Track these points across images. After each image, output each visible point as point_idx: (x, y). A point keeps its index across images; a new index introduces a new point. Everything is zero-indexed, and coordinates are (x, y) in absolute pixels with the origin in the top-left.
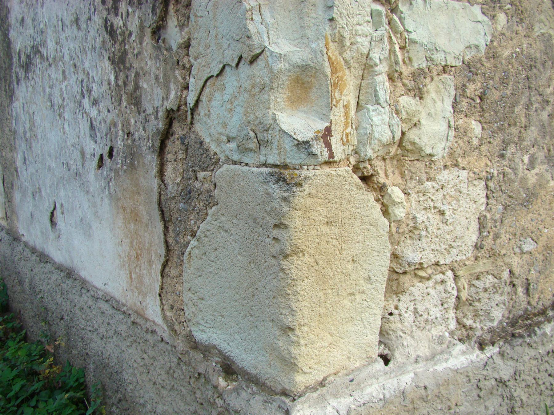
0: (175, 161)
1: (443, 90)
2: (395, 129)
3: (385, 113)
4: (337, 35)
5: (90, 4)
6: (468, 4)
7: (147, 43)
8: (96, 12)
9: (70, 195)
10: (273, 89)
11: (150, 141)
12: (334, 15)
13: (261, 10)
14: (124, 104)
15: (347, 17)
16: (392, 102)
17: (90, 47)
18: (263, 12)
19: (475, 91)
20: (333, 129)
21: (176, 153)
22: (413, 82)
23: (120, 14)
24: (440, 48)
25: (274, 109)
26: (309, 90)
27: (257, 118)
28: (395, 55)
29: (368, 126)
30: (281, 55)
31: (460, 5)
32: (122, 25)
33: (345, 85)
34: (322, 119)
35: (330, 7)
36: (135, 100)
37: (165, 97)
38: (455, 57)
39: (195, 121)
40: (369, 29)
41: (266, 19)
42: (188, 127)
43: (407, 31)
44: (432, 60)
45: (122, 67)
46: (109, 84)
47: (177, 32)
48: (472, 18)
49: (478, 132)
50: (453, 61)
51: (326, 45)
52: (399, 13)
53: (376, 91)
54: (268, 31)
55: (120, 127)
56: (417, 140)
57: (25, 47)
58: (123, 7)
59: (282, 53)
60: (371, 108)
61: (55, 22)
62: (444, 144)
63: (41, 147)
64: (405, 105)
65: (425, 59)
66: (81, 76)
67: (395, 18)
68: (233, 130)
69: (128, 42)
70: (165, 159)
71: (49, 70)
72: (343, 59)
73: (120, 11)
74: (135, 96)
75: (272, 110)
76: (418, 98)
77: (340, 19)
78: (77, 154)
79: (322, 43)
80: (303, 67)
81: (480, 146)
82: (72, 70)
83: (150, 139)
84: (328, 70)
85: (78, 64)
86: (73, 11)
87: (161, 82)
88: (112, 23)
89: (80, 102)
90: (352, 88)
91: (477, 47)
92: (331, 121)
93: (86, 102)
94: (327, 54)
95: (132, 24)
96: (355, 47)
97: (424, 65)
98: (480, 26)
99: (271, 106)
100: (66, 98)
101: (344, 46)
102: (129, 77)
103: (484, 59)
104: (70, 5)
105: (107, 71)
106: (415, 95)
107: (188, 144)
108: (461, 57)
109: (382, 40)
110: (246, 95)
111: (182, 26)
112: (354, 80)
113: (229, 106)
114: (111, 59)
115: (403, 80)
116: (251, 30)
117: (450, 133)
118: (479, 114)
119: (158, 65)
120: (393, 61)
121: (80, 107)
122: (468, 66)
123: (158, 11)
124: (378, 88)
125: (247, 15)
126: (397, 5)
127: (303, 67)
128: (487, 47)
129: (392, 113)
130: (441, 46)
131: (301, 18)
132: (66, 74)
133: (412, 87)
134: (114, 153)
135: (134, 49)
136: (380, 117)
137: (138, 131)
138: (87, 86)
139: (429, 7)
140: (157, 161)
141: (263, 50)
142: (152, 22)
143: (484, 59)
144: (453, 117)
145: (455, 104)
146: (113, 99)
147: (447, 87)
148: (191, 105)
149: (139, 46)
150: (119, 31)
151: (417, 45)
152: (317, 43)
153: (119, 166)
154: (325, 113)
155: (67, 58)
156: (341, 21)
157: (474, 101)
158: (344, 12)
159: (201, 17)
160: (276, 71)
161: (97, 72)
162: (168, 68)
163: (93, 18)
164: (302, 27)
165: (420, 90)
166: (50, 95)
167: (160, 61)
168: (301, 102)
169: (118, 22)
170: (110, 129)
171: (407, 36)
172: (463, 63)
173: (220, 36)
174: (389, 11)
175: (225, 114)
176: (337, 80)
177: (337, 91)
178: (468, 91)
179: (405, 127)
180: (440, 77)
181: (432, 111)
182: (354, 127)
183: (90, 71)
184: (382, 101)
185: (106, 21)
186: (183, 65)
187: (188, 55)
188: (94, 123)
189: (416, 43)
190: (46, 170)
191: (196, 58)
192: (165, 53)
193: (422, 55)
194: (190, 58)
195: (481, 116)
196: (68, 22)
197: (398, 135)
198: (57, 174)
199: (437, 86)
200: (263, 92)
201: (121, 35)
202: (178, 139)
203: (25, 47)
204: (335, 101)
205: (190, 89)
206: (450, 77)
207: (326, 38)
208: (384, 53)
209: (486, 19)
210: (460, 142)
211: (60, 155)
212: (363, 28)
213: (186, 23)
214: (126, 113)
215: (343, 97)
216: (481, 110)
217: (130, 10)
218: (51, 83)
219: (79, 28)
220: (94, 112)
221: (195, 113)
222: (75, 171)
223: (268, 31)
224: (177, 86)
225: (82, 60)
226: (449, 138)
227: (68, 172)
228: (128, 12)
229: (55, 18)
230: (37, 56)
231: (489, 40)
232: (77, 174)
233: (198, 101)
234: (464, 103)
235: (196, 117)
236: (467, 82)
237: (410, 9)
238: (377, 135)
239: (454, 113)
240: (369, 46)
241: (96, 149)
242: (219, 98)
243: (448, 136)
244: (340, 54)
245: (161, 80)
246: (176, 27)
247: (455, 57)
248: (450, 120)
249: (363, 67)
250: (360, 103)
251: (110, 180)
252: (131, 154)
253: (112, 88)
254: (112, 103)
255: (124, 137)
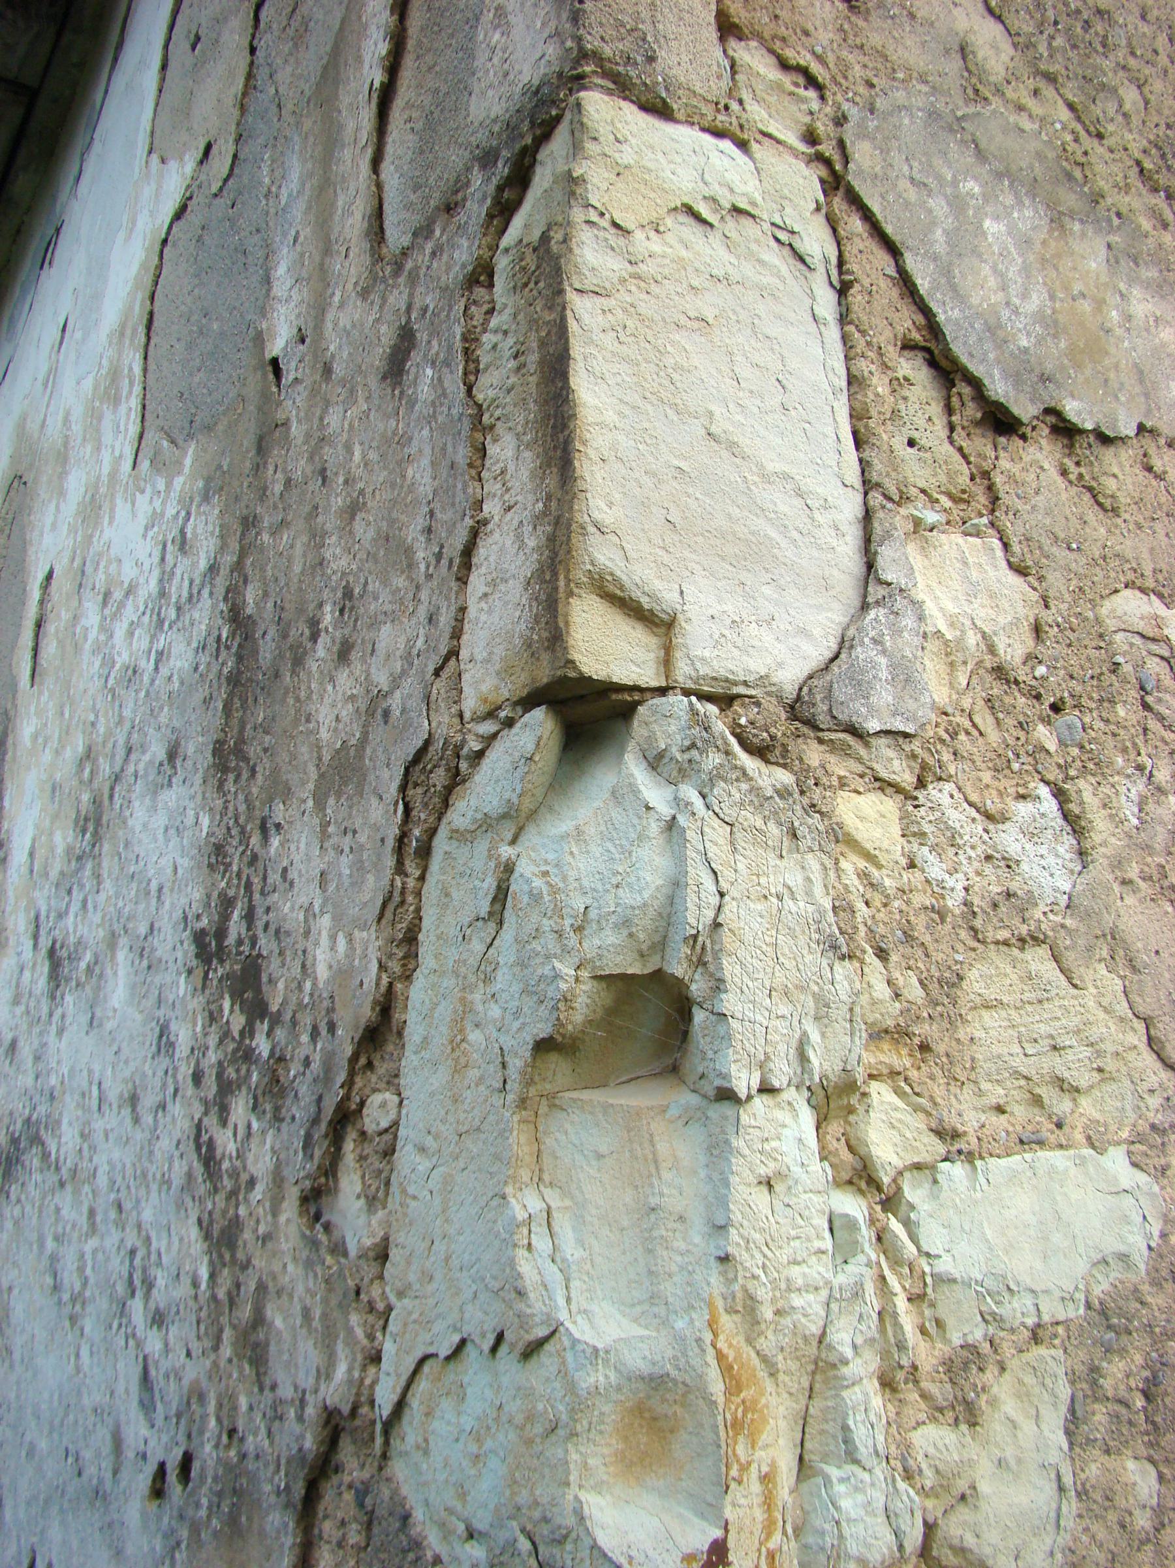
0: (340, 1545)
1: (1037, 1390)
2: (904, 1523)
3: (873, 1484)
4: (739, 1295)
5: (166, 1072)
6: (1092, 1152)
7: (288, 1220)
8: (178, 1099)
9: (75, 1544)
10: (577, 1435)
11: (282, 1473)
12: (730, 1249)
13: (553, 1224)
14: (227, 1351)
15: (765, 1249)
16: (893, 1449)
17: (158, 1176)
18: (556, 1228)
19: (1128, 1376)
20: (731, 1543)
21: (343, 1523)
22: (948, 1386)
23: (231, 1126)
24: (1018, 1284)
25: (580, 1487)
26: (668, 1435)
27: (538, 1504)
28: (897, 1325)
29: (827, 1526)
30: (596, 1350)
31: (1069, 1158)
32: (234, 1154)
33: (764, 1420)
34: (702, 1516)
35: (721, 1227)
36: (253, 1350)
37: (323, 1370)
38: (1063, 1299)
39: (392, 1453)
40: (822, 1270)
41: (564, 1246)
42: (376, 1464)
43: (928, 1255)
44: (998, 1319)
45: (227, 1257)
46: (195, 1284)
47: (360, 1209)
48: (1103, 1186)
49: (1146, 1491)
50: (1060, 1308)
51: (712, 1325)
52: (904, 1208)
53: (845, 1428)
54: (567, 1280)
55: (212, 1407)
56: (970, 1541)
57: (11, 1114)
58: (240, 1110)
59: (600, 1346)
60: (834, 1472)
61: (85, 1084)
62: (1049, 1541)
63: (18, 1383)
64: (931, 1451)
65: (979, 1318)
66: (132, 1239)
67: (895, 1225)
68: (480, 1513)
69: (245, 1198)
70: (316, 1531)
71: (57, 1195)
72: (758, 1353)
73: (233, 1119)
74: (253, 1338)
75: (574, 1489)
76: (964, 1427)
77: (745, 1256)
78: (103, 1436)
79: (700, 1318)
80: (651, 1380)
81: (1157, 1530)
82: (113, 1214)
83: (283, 1468)
84: (717, 1387)
85: (127, 1205)
86: (127, 1073)
87: (316, 1330)
88: (211, 1139)
89: (124, 1304)
90: (782, 1424)
91: (1123, 1257)
92: (727, 1523)
93: (137, 1306)
94: (714, 1346)
95: (256, 1161)
96: (787, 1321)
97: (977, 1334)
98: (1128, 1201)
99: (572, 1478)
100: (92, 1281)
101: (758, 1323)
102: (243, 1288)
103: (1145, 1288)
104: (123, 1057)
105: (192, 1251)
106: (956, 1419)
107: (373, 1511)
108: (1080, 1296)
109: (857, 1293)
110: (512, 1436)
111: (373, 1201)
112: (788, 1403)
113: (473, 1448)
114: (205, 1224)
115: (923, 1384)
116: (526, 1276)
117: (1064, 1509)
118: (1146, 1438)
119: (311, 1285)
120: (892, 1340)
121: (121, 1316)
122: (1104, 1313)
123: (318, 1153)
124: (851, 1423)
125: (516, 1237)
126: (899, 1189)
127: (651, 1380)
128: (1153, 1255)
129: (894, 1481)
130: (1020, 1278)
131: (650, 1251)
132: (99, 1218)
133: (946, 1400)
134: (193, 1474)
135: (258, 1221)
136: (860, 1498)
137: (256, 1434)
138: (144, 1270)
139: (983, 1181)
140: (295, 1536)
141: (553, 1333)
142: (302, 1174)
143: (1145, 1288)
144: (1068, 1462)
145: (1073, 1423)
146: (202, 1327)
147: (1048, 1381)
148: (386, 1413)
149: (269, 1218)
150: (226, 1165)
151: (955, 1287)
152: (687, 1318)
153: (203, 1513)
154: (709, 1498)
155: (102, 1180)
156: (749, 1261)
157: (1127, 1406)
158: (757, 1236)
159: (415, 1198)
160: (584, 1393)
161: (169, 1244)
162: (334, 1302)
163: (169, 1106)
164: (651, 1273)
165: (969, 1406)
166: (54, 1258)
167: (316, 1275)
168: (651, 1465)
169: (226, 1142)
170: (188, 1403)
171: (927, 1269)
172: (1088, 1306)
173: (455, 1262)
174: (878, 1208)
175: (464, 1463)
176: (740, 1410)
177: (741, 1438)
178: (1107, 1384)
179: (935, 1508)
180: (1028, 1357)
181: (1009, 1453)
182: (790, 1531)
183: (153, 1235)
184: (863, 1452)
185: (199, 1127)
186: (369, 1302)
187: (381, 1277)
188: (153, 1372)
189: (954, 1281)
190: (24, 1453)
191: (400, 1294)
192: (329, 1260)
193: (970, 1309)
194: (388, 1289)
195: (1150, 1444)
196: (112, 1095)
197: (914, 1536)
198: (49, 1474)
199: (1020, 1382)
200: (553, 1438)
201: (230, 1176)
202: (350, 1487)
203: (11, 1114)
204: (735, 1467)
205: (385, 1364)
206: (1053, 1352)
207: (711, 1305)
208: (863, 1328)
209: (1142, 1178)
210: (1095, 1528)
211: (62, 1424)
212: (807, 1270)
213: (381, 1194)
214: (230, 1376)
215: (760, 1454)
216: (1150, 1427)
217: (255, 1125)
218: (60, 1230)
219: (136, 1120)
220: (154, 1343)
221: (394, 1433)
222: (95, 1482)
223: (567, 1280)
224: (354, 1353)
225: (138, 1201)
226: (1062, 1523)
227: (76, 1479)
228: (249, 1126)
229: (85, 1073)
230: (34, 1150)
231: (1156, 1234)
232: (98, 1494)
233: (400, 1406)
234: (1097, 1417)
235: (395, 1443)
236: (1102, 1359)
237: (934, 1197)
238: (853, 1547)
239: (1071, 1449)
240: (823, 1314)
241: (152, 1443)
242: (450, 1416)
243: (1058, 1516)
244: (749, 1341)
245: (316, 1323)
246: (358, 1197)
247: (1063, 1299)
248: (1062, 1471)
249: (811, 1367)
250: (806, 1457)
251: (178, 1544)
252: (235, 1491)
253: (200, 1297)
254: (199, 1338)
255: (220, 1437)
